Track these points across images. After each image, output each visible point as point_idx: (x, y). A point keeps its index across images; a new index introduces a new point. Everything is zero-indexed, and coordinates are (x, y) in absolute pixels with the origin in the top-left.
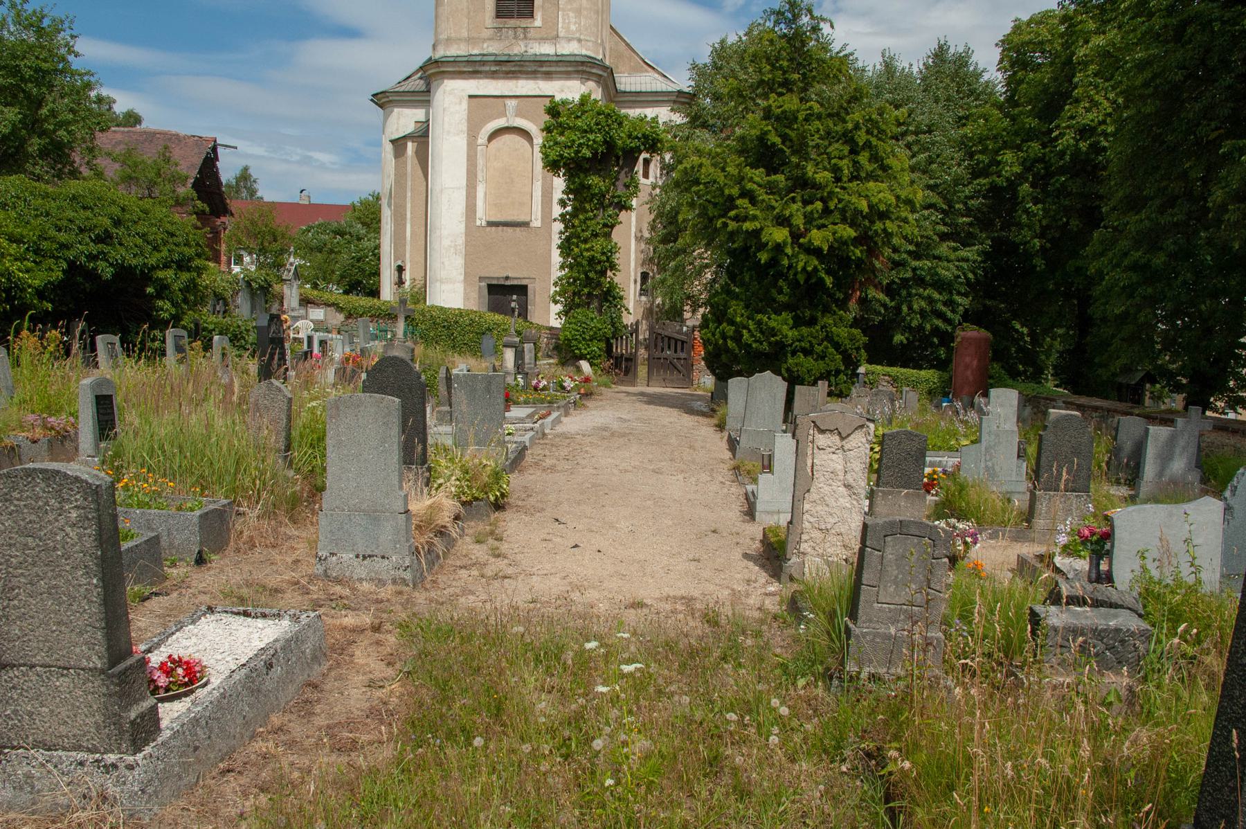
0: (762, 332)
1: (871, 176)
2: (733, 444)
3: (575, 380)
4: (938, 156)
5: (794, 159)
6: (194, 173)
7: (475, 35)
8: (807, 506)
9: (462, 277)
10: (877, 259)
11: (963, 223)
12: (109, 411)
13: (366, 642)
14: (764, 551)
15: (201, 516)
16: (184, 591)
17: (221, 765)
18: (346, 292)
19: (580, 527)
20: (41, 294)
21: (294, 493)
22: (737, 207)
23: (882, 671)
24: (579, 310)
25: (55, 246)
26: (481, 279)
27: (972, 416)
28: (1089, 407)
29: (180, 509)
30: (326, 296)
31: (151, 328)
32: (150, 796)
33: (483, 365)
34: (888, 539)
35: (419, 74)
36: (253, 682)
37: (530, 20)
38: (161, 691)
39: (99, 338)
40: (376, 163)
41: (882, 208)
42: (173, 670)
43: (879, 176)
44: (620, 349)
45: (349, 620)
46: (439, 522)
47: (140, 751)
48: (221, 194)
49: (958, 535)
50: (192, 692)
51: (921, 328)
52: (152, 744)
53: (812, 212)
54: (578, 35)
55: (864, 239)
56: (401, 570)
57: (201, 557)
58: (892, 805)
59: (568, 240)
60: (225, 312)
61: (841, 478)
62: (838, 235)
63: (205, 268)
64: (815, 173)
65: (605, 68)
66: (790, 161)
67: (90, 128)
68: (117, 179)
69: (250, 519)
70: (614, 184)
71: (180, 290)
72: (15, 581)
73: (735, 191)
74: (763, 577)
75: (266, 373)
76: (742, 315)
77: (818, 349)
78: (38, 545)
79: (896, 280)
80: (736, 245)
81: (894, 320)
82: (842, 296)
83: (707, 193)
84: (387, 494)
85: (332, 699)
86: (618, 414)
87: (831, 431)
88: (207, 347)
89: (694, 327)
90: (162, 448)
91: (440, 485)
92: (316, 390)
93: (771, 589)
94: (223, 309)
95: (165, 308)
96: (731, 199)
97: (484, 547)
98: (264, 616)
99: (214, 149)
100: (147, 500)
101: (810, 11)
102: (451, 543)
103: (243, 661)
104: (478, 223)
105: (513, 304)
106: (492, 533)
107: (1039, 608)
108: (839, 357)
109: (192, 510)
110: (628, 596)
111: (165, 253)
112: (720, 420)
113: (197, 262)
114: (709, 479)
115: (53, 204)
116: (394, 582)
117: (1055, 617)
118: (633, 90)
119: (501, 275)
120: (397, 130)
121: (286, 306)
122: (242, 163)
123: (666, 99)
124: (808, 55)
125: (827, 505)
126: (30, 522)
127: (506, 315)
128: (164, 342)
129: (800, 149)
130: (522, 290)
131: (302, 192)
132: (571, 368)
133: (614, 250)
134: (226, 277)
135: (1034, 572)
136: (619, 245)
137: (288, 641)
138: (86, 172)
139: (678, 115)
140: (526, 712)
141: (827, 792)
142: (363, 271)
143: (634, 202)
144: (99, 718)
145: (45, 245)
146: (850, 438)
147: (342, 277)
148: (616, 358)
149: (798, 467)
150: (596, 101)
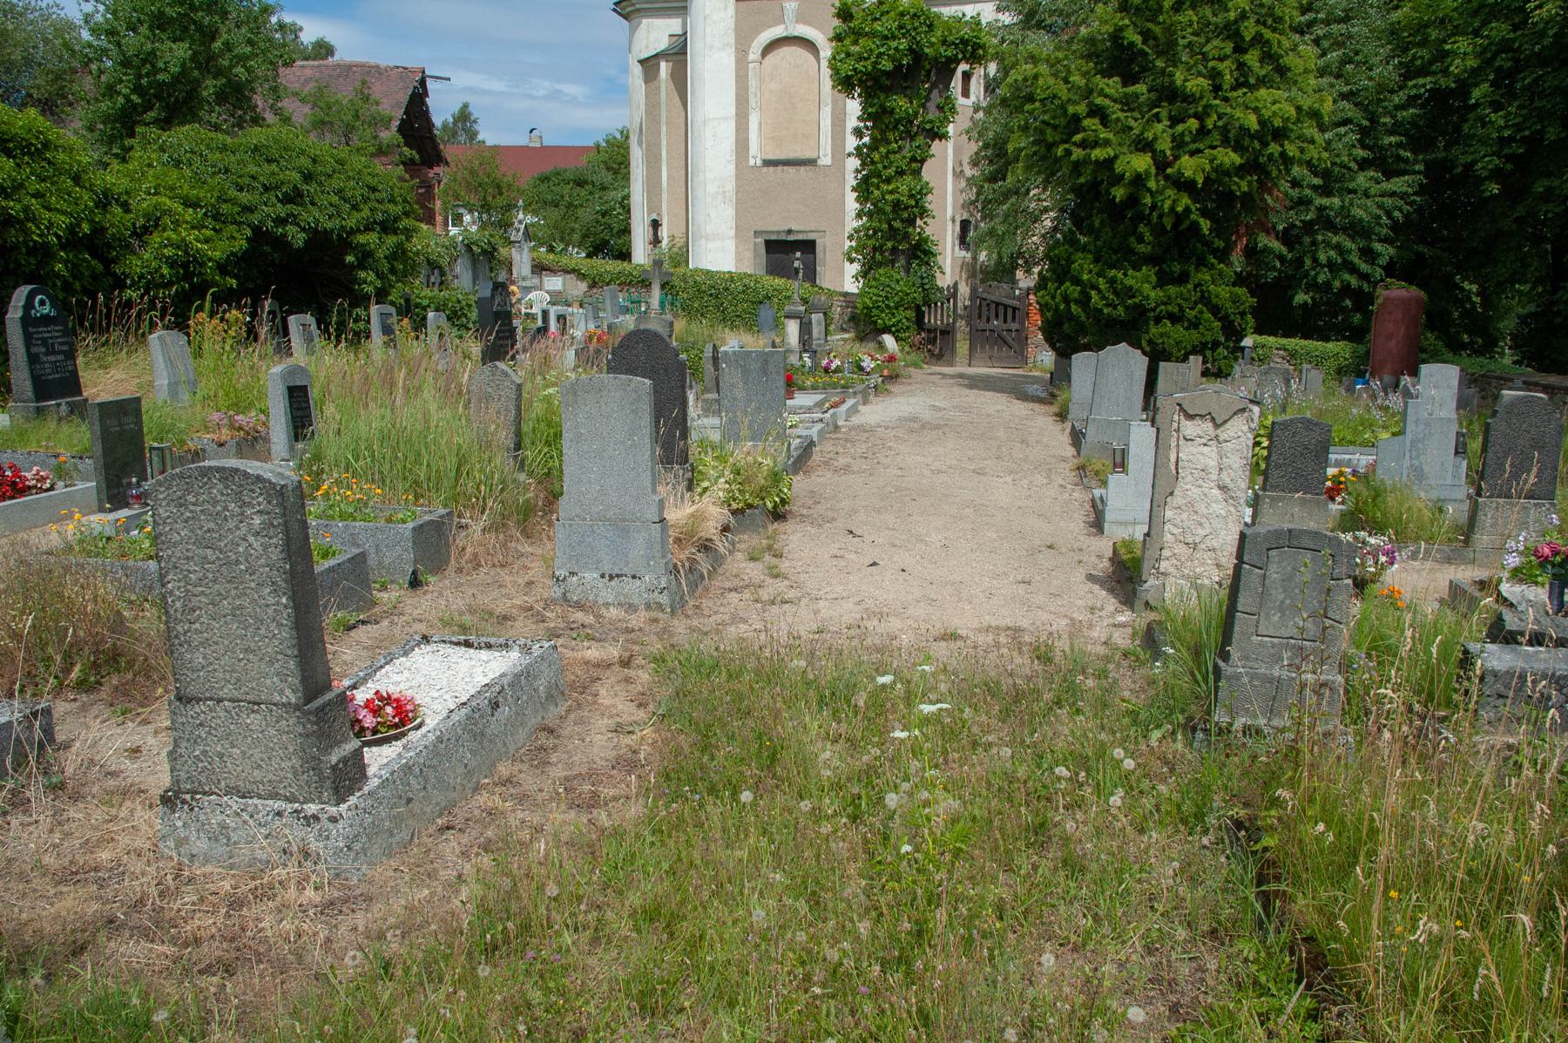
0: (1116, 293)
1: (1263, 82)
2: (1077, 438)
4: (1357, 53)
5: (1160, 64)
6: (399, 114)
8: (1169, 514)
9: (732, 233)
10: (1270, 194)
11: (1390, 144)
12: (304, 405)
13: (613, 679)
14: (1113, 573)
15: (414, 529)
17: (439, 821)
18: (589, 256)
20: (222, 268)
21: (528, 501)
22: (1084, 130)
23: (1262, 722)
24: (881, 271)
25: (237, 209)
27: (1395, 400)
28: (1560, 388)
29: (389, 520)
30: (564, 260)
31: (353, 305)
32: (357, 853)
34: (1273, 553)
38: (368, 732)
39: (292, 319)
41: (1278, 123)
42: (381, 708)
44: (933, 319)
45: (593, 653)
46: (702, 534)
47: (344, 801)
48: (432, 138)
49: (1369, 553)
50: (404, 734)
51: (1328, 284)
52: (358, 794)
53: (1182, 134)
55: (1252, 167)
56: (656, 593)
57: (416, 578)
58: (1263, 888)
59: (866, 180)
60: (441, 283)
61: (1214, 477)
64: (1186, 80)
66: (1154, 66)
67: (271, 63)
69: (474, 533)
70: (923, 106)
72: (195, 602)
73: (1082, 109)
74: (1111, 603)
76: (1090, 272)
78: (218, 558)
79: (1298, 223)
80: (1082, 180)
81: (1294, 275)
85: (571, 746)
86: (930, 401)
87: (1202, 416)
88: (420, 325)
89: (1029, 289)
90: (369, 448)
91: (705, 490)
93: (1121, 618)
95: (368, 280)
96: (1076, 119)
97: (760, 565)
98: (489, 646)
99: (423, 82)
100: (351, 510)
102: (718, 560)
103: (464, 699)
104: (752, 162)
105: (796, 264)
106: (770, 548)
107: (1474, 647)
108: (1217, 324)
109: (404, 522)
110: (938, 625)
111: (366, 213)
113: (405, 223)
114: (1045, 481)
115: (233, 159)
116: (648, 607)
117: (1496, 658)
120: (647, 47)
121: (515, 275)
125: (1196, 512)
126: (209, 531)
128: (368, 322)
129: (1168, 49)
130: (809, 247)
132: (872, 345)
133: (924, 191)
134: (441, 240)
135: (1473, 602)
136: (930, 185)
137: (517, 676)
138: (270, 118)
139: (1007, 14)
140: (805, 764)
141: (1182, 870)
144: (295, 761)
145: (225, 208)
147: (585, 236)
148: (929, 331)
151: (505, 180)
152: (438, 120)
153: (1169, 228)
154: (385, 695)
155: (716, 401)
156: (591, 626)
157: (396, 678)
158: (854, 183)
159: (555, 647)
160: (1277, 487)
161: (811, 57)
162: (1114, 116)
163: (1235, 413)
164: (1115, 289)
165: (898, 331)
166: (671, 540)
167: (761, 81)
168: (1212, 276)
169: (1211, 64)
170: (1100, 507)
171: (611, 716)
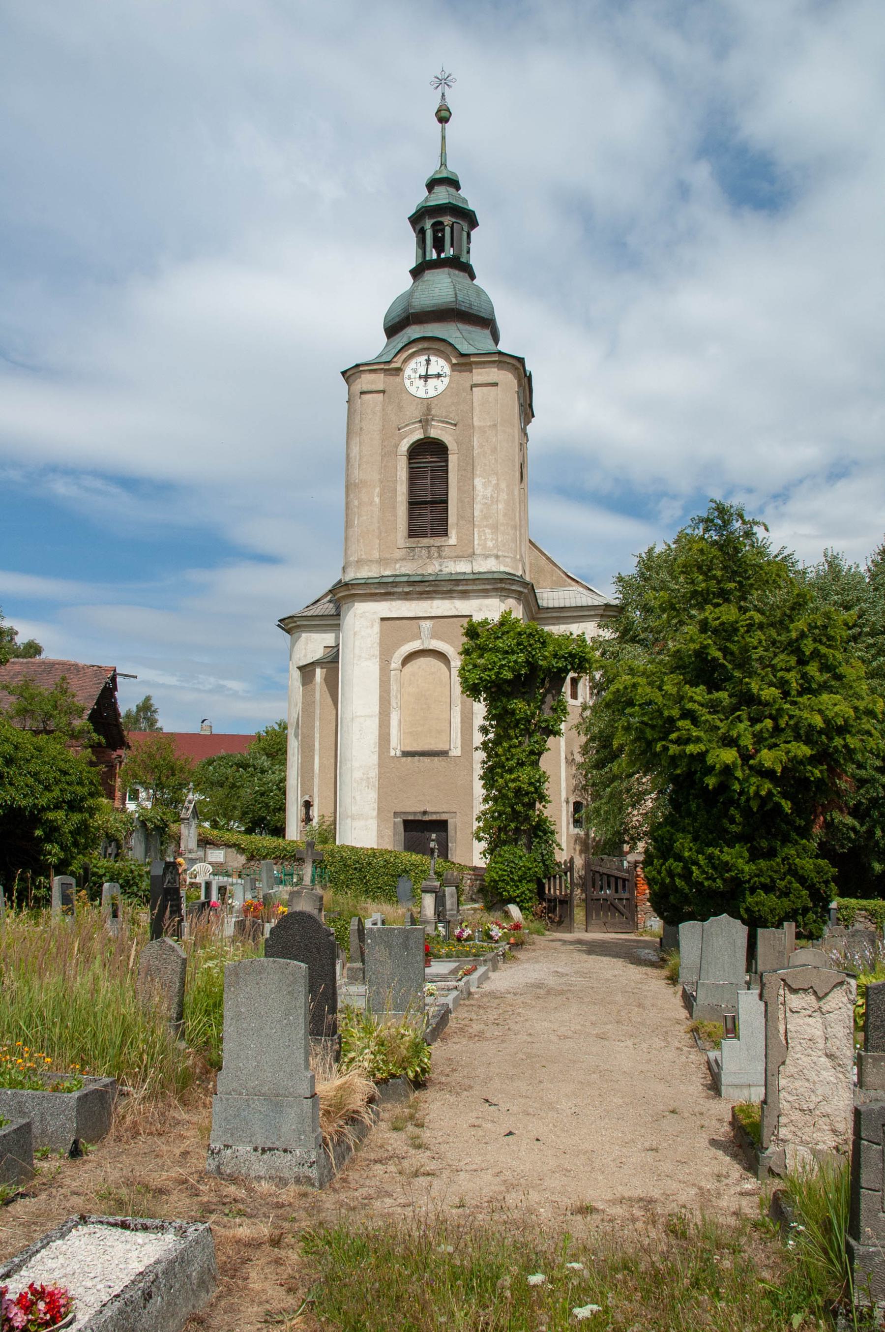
0: (714, 868)
1: (825, 687)
2: (689, 1001)
3: (504, 928)
5: (737, 674)
6: (91, 704)
7: (388, 556)
8: (783, 1082)
9: (375, 813)
13: (263, 1260)
14: (735, 1136)
15: (79, 1098)
16: (54, 1191)
18: (249, 831)
19: (514, 1109)
21: (187, 1068)
22: (678, 729)
24: (505, 848)
26: (396, 814)
29: (56, 1089)
30: (227, 836)
31: (37, 873)
33: (400, 911)
35: (329, 598)
36: (126, 1319)
37: (444, 538)
40: (281, 690)
41: (840, 722)
43: (832, 686)
44: (553, 890)
45: (244, 1231)
46: (350, 1107)
48: (118, 725)
53: (761, 731)
54: (495, 552)
55: (823, 757)
56: (306, 1167)
59: (491, 769)
60: (117, 855)
61: (821, 1046)
62: (792, 754)
63: (98, 808)
65: (525, 584)
68: (12, 712)
70: (539, 708)
71: (70, 832)
73: (675, 713)
74: (736, 1170)
75: (157, 930)
76: (691, 849)
77: (782, 884)
80: (678, 771)
82: (803, 823)
83: (643, 715)
84: (291, 1075)
86: (553, 968)
87: (805, 990)
88: (95, 894)
89: (636, 863)
91: (352, 1060)
92: (212, 949)
94: (115, 852)
95: (53, 852)
96: (671, 720)
97: (402, 1135)
98: (145, 1228)
99: (113, 679)
100: (21, 1078)
101: (741, 516)
102: (363, 1132)
103: (117, 1290)
104: (392, 753)
105: (432, 844)
106: (412, 1117)
108: (805, 892)
109: (70, 1091)
110: (575, 1197)
111: (56, 793)
112: (672, 971)
114: (663, 1044)
116: (298, 1181)
118: (557, 605)
119: (418, 810)
120: (305, 656)
121: (182, 848)
122: (146, 691)
123: (592, 613)
124: (740, 563)
125: (808, 1080)
127: (424, 854)
128: (50, 889)
129: (743, 663)
130: (441, 826)
131: (203, 722)
132: (499, 914)
136: (547, 775)
137: (172, 1262)
142: (267, 806)
143: (563, 726)
146: (828, 998)
147: (244, 813)
148: (550, 901)
149: (769, 1034)
150: (518, 621)
151: (178, 763)
152: (123, 710)
153: (755, 810)
154: (39, 1288)
155: (360, 969)
156: (242, 1201)
157: (51, 1264)
158: (481, 772)
159: (210, 1230)
160: (878, 1047)
161: (443, 666)
162: (703, 718)
163: (835, 987)
164: (713, 864)
165: (522, 901)
166: (321, 1113)
167: (401, 686)
168: (797, 851)
169: (779, 674)
170: (716, 1070)
171: (260, 1303)
